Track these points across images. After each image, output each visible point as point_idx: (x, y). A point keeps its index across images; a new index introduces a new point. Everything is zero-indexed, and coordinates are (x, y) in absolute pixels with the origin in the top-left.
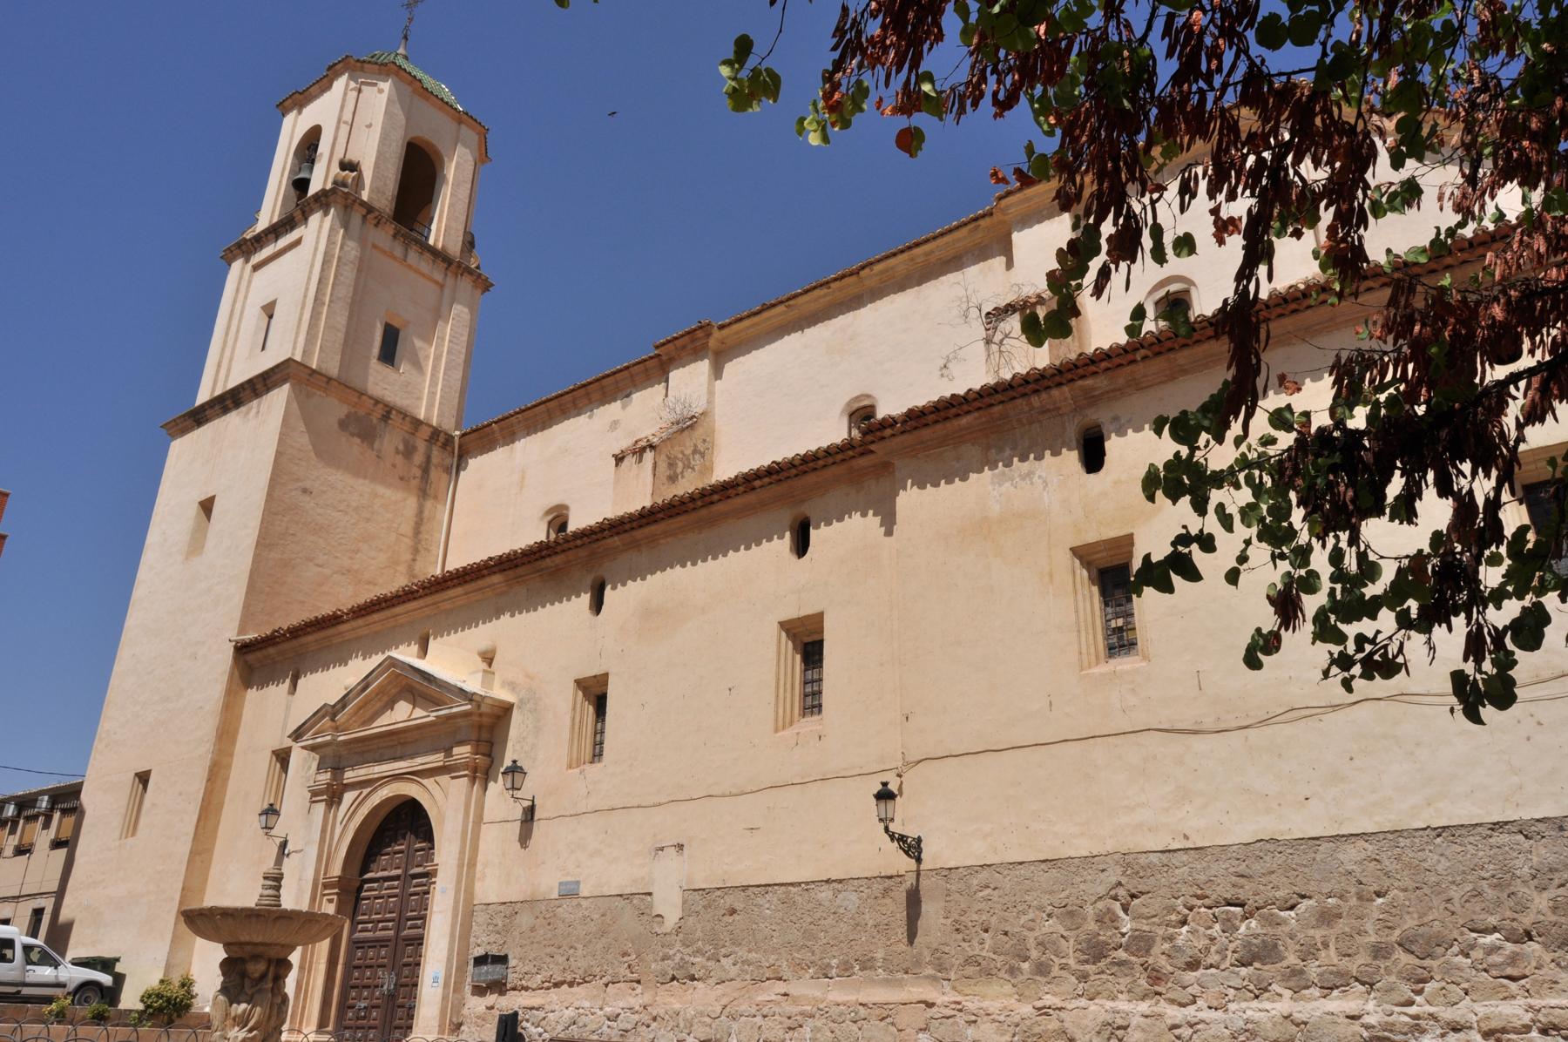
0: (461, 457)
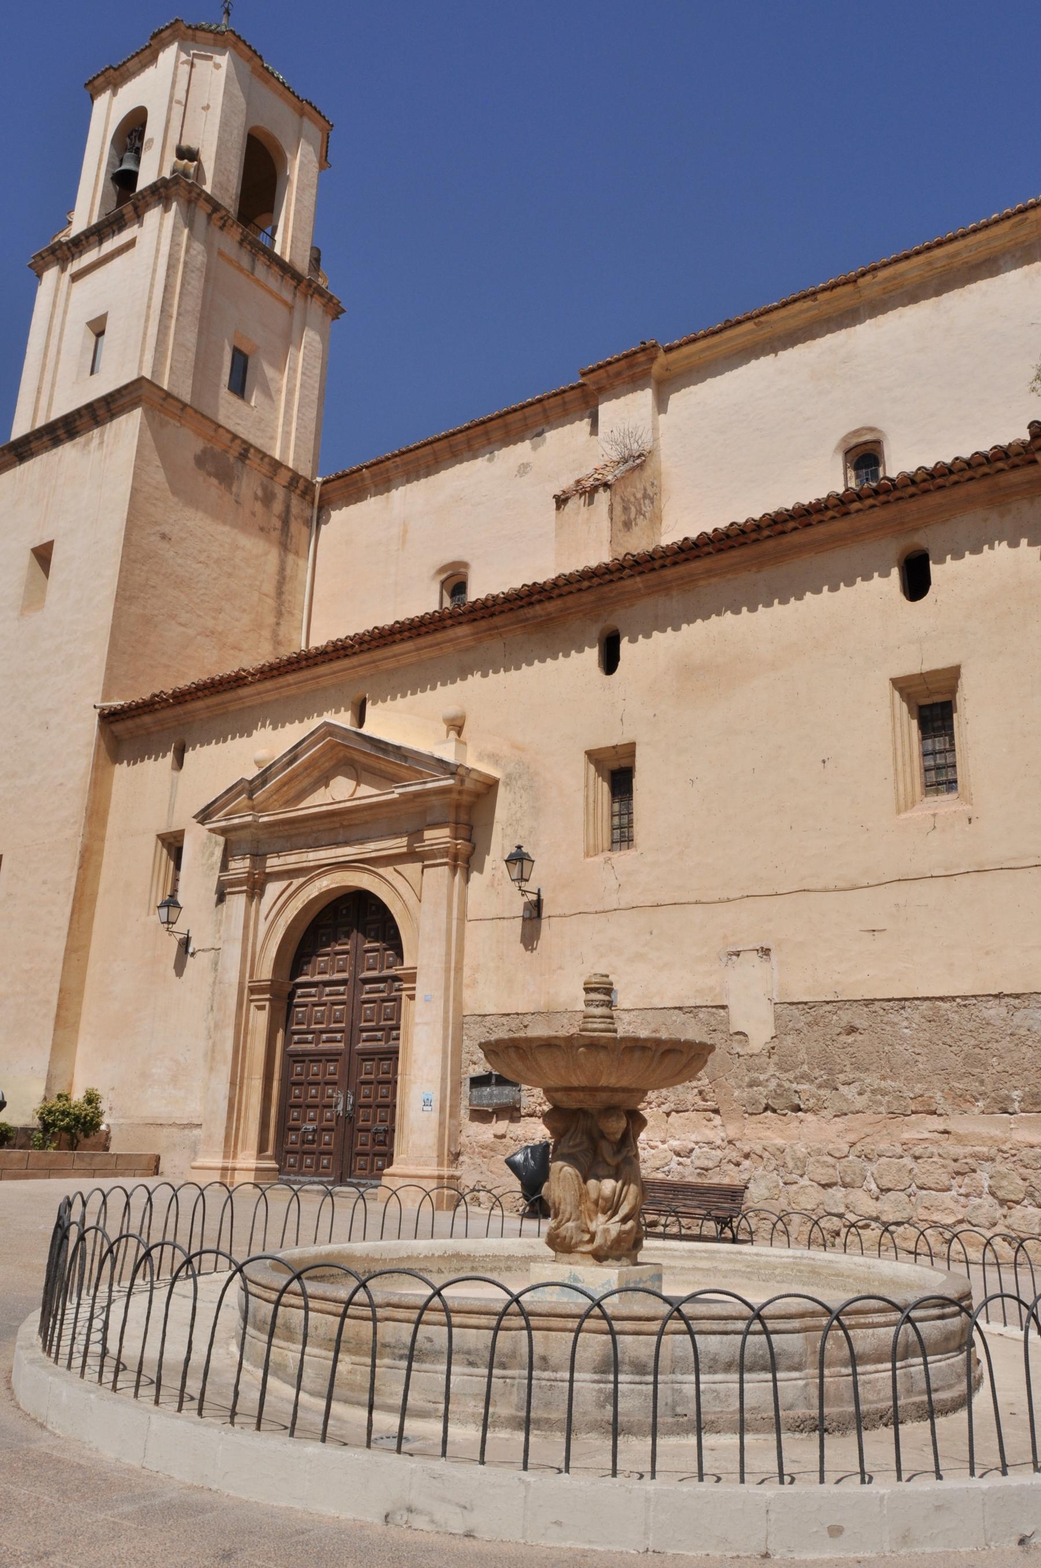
0: (320, 508)
